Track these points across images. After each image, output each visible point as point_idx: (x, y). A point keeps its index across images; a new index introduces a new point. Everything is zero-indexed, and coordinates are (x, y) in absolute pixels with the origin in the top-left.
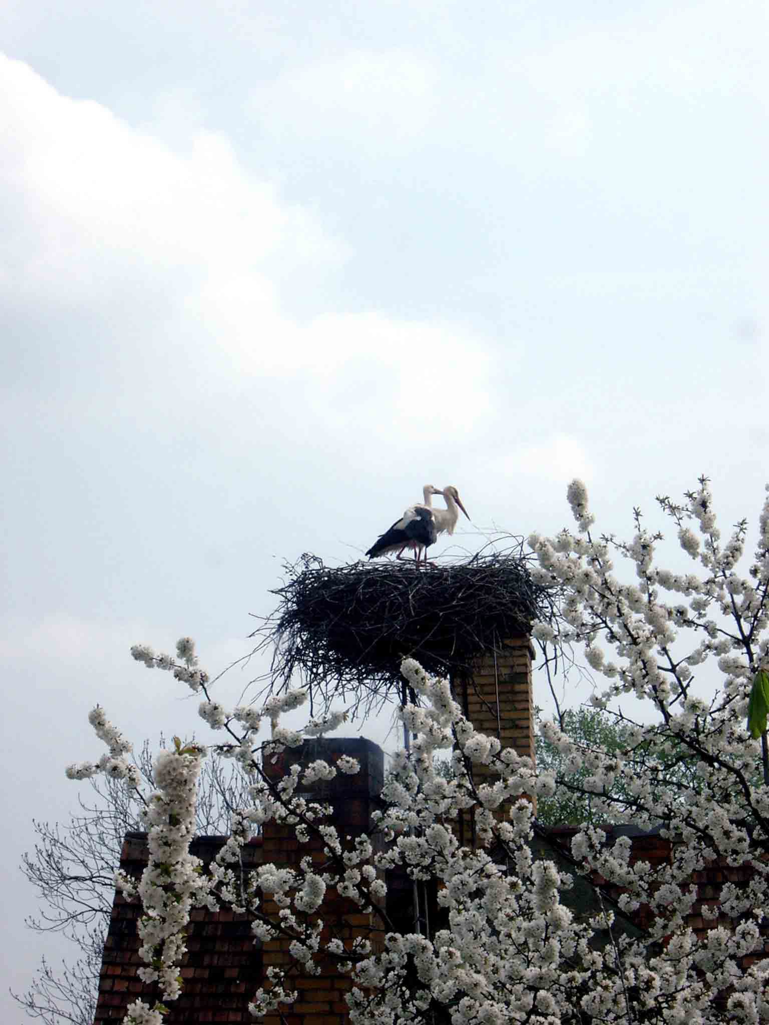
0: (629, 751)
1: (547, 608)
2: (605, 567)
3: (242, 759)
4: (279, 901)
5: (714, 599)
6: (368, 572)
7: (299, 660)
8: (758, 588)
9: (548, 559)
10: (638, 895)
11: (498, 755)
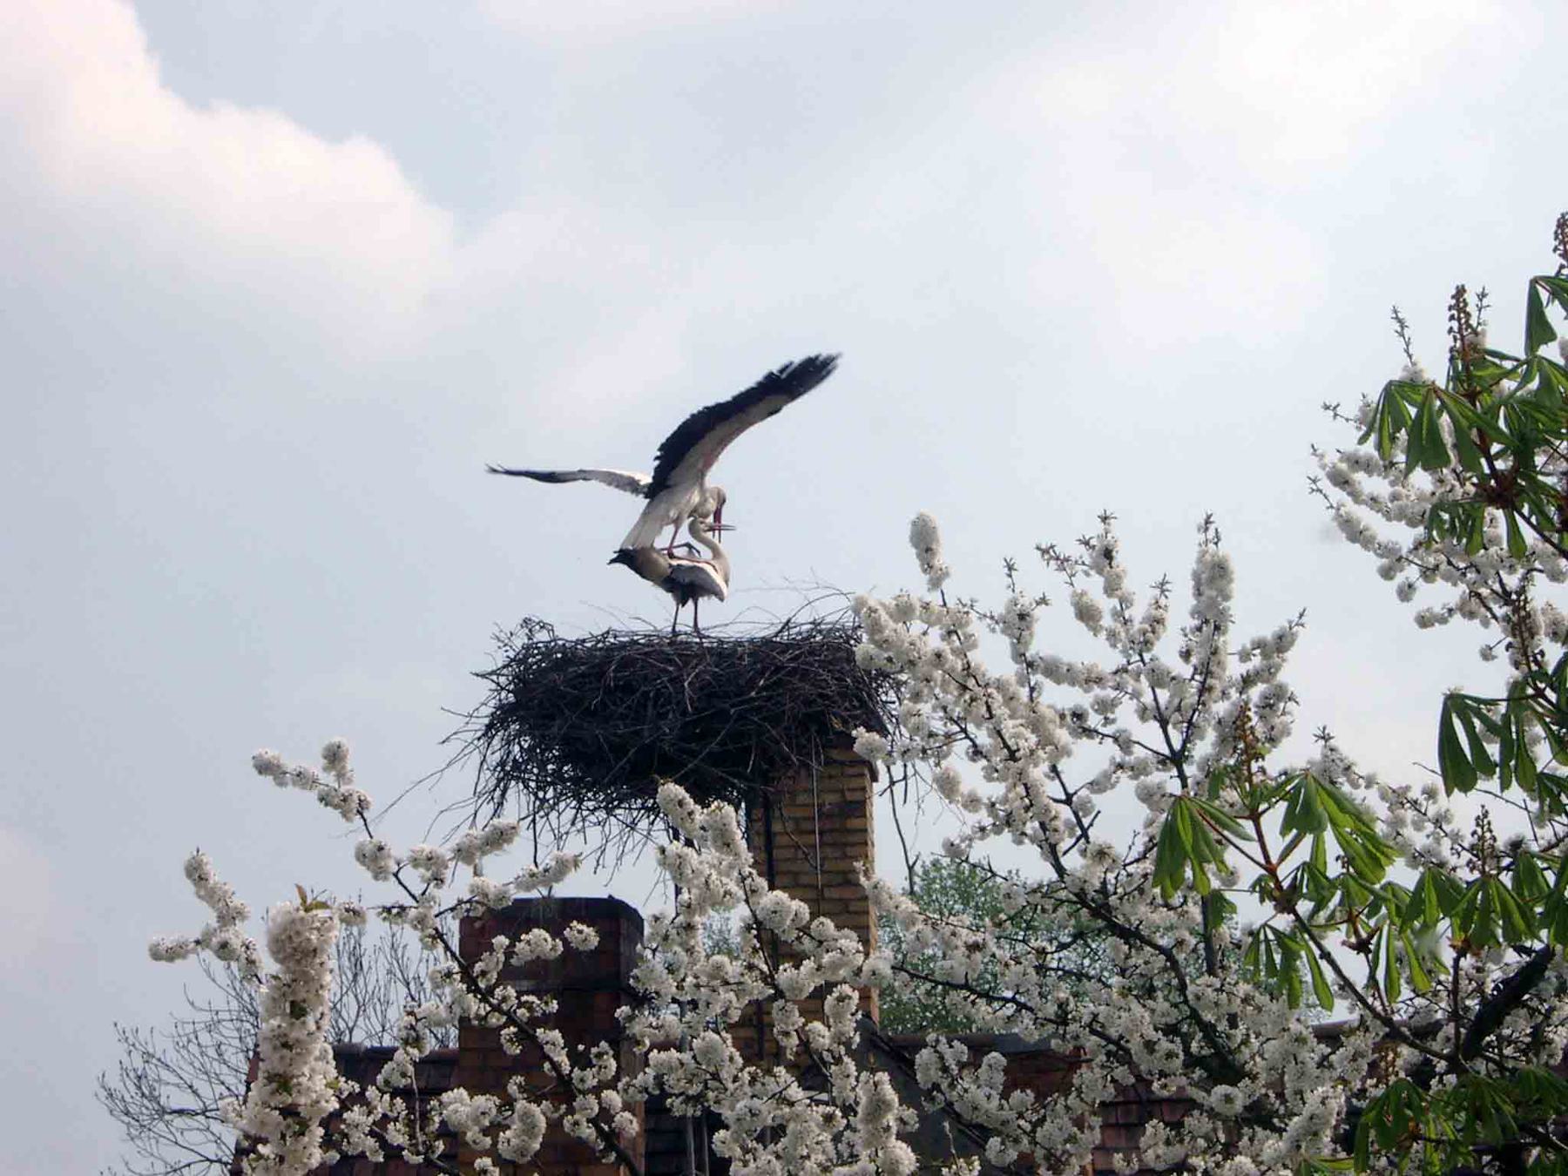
0: (1005, 921)
1: (894, 703)
2: (969, 643)
3: (419, 927)
4: (474, 1142)
5: (1128, 696)
6: (623, 646)
7: (518, 779)
8: (1193, 678)
9: (881, 631)
10: (1016, 1141)
11: (805, 930)
